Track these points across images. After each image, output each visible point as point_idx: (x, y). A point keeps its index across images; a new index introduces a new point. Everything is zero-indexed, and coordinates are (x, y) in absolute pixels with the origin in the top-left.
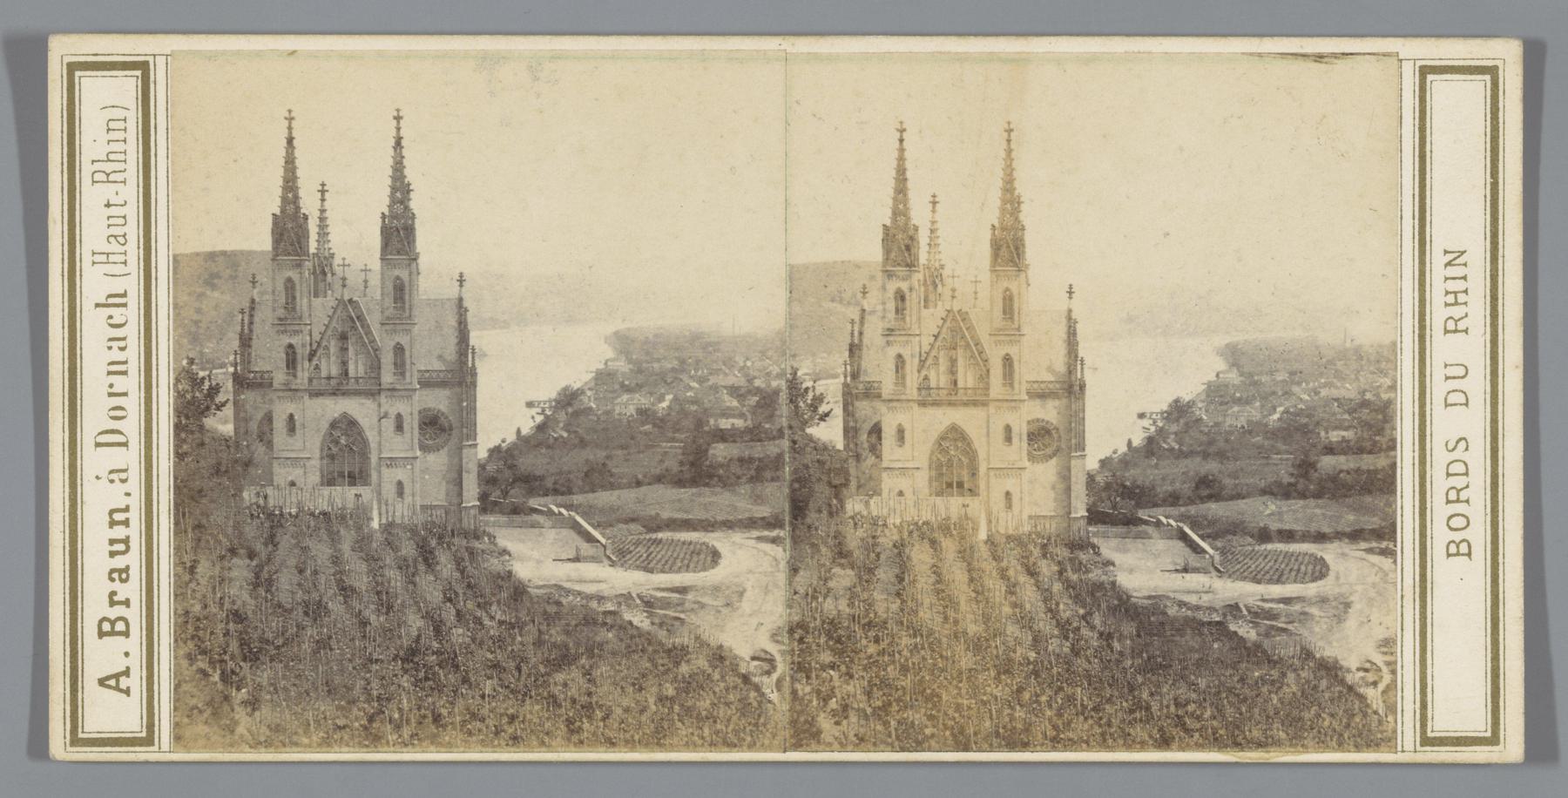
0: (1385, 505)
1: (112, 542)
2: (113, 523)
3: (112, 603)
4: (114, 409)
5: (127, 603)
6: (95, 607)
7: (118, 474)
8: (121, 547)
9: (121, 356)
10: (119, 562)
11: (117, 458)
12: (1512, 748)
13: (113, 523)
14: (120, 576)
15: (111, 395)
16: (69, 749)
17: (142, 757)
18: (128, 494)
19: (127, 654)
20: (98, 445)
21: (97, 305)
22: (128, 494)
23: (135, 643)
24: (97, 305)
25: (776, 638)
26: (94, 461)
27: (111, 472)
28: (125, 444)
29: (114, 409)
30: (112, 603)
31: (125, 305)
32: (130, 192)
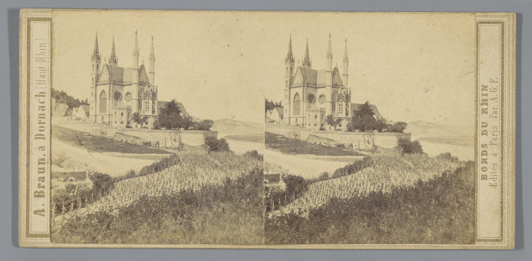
0: (297, 181)
1: (39, 169)
2: (39, 163)
3: (39, 187)
4: (40, 127)
5: (44, 187)
6: (34, 188)
7: (42, 148)
8: (42, 171)
9: (43, 112)
10: (42, 175)
11: (41, 143)
12: (508, 241)
13: (39, 163)
14: (41, 180)
15: (39, 123)
16: (503, 242)
17: (302, 248)
18: (44, 155)
19: (43, 205)
20: (36, 138)
21: (36, 96)
22: (44, 155)
23: (33, 208)
24: (36, 96)
25: (483, 169)
26: (35, 144)
27: (39, 147)
28: (44, 138)
29: (40, 127)
30: (39, 187)
31: (45, 96)
32: (47, 65)
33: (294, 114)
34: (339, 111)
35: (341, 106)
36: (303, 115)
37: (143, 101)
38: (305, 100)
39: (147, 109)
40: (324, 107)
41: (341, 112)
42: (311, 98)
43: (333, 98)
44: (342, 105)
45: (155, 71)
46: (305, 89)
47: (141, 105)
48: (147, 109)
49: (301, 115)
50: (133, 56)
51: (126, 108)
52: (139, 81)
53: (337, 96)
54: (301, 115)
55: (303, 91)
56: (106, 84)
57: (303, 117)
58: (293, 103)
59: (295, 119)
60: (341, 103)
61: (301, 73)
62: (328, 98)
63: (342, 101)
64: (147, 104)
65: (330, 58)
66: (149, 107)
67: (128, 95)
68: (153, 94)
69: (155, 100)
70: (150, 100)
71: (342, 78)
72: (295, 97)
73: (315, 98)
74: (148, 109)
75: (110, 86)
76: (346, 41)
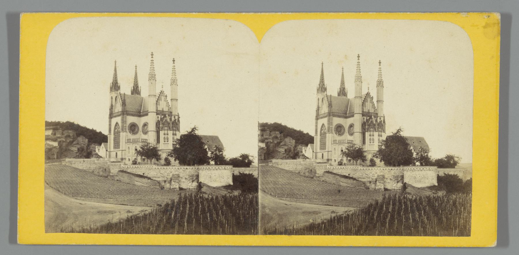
34: (370, 143)
54: (327, 150)
56: (119, 116)
57: (328, 151)
60: (372, 133)
74: (168, 142)
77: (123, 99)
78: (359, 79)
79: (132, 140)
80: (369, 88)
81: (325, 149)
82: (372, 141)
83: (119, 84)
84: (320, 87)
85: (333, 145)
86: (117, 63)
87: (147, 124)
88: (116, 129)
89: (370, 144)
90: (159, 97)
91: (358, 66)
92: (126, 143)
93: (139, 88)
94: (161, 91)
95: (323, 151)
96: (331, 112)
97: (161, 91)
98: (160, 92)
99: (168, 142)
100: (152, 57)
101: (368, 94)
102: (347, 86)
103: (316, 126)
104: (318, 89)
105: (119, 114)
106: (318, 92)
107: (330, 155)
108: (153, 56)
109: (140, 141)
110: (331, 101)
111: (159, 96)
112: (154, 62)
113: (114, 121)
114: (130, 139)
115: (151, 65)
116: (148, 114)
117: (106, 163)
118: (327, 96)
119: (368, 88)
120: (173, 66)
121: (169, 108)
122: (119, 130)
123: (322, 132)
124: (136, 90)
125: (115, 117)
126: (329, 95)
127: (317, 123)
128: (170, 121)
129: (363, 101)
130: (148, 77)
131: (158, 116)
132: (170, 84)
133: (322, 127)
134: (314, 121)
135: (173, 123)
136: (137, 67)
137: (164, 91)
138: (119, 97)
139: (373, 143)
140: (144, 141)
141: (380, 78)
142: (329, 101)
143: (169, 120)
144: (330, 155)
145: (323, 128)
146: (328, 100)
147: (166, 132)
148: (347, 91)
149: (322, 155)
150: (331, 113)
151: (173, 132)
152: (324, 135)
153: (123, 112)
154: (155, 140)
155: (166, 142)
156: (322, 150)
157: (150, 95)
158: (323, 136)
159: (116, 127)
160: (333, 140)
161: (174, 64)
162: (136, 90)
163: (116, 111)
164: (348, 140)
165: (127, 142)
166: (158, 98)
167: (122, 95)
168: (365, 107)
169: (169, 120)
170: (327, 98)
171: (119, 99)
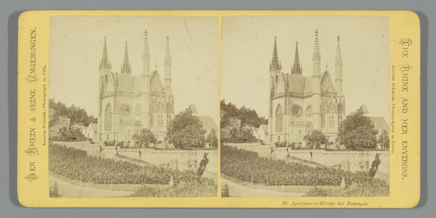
33: (276, 131)
34: (159, 124)
35: (161, 118)
36: (286, 131)
37: (155, 114)
38: (288, 113)
39: (332, 125)
40: (311, 121)
41: (160, 125)
42: (296, 110)
43: (151, 108)
44: (333, 117)
45: (343, 79)
46: (288, 100)
47: (324, 120)
48: (332, 125)
49: (284, 132)
50: (335, 65)
51: (305, 124)
52: (321, 91)
53: (326, 106)
54: (284, 132)
55: (286, 102)
56: (282, 97)
57: (286, 134)
58: (104, 116)
59: (277, 136)
60: (160, 114)
61: (283, 81)
62: (316, 109)
63: (333, 113)
64: (332, 119)
65: (317, 60)
66: (334, 122)
67: (310, 109)
68: (338, 106)
69: (341, 113)
70: (163, 113)
71: (334, 85)
72: (277, 110)
73: (302, 110)
74: (333, 125)
75: (286, 99)
76: (339, 38)
77: (115, 79)
78: (317, 57)
79: (125, 122)
80: (328, 67)
81: (281, 130)
82: (332, 123)
83: (109, 61)
84: (274, 64)
85: (120, 126)
86: (106, 39)
87: (311, 107)
88: (278, 111)
89: (330, 126)
90: (323, 78)
91: (146, 43)
92: (118, 125)
93: (301, 67)
94: (326, 71)
95: (109, 132)
96: (288, 92)
97: (155, 71)
98: (154, 71)
99: (162, 124)
100: (317, 35)
101: (326, 73)
102: (131, 63)
103: (271, 107)
104: (271, 66)
105: (282, 95)
106: (271, 69)
107: (116, 137)
108: (318, 34)
109: (304, 124)
110: (288, 81)
111: (323, 76)
112: (318, 40)
113: (276, 102)
114: (294, 122)
115: (316, 44)
116: (312, 95)
117: (263, 148)
118: (283, 75)
119: (156, 65)
120: (167, 44)
121: (163, 88)
122: (281, 112)
123: (278, 113)
124: (297, 69)
125: (107, 97)
126: (114, 73)
127: (101, 102)
128: (165, 102)
129: (321, 81)
130: (313, 57)
131: (152, 97)
132: (164, 63)
133: (278, 107)
134: (98, 99)
135: (167, 105)
136: (127, 44)
137: (157, 71)
138: (111, 76)
139: (162, 124)
140: (308, 125)
141: (168, 55)
142: (286, 79)
143: (163, 102)
144: (116, 137)
145: (278, 109)
146: (284, 79)
147: (332, 115)
148: (302, 68)
149: (278, 137)
150: (288, 93)
151: (167, 114)
152: (280, 116)
153: (116, 92)
154: (149, 122)
155: (160, 125)
156: (278, 132)
157: (143, 76)
158: (279, 117)
159: (278, 109)
160: (290, 122)
161: (167, 42)
162: (297, 69)
163: (278, 92)
164: (306, 121)
165: (290, 125)
166: (322, 78)
167: (114, 75)
168: (153, 86)
169: (163, 102)
170: (283, 77)
171: (281, 80)
